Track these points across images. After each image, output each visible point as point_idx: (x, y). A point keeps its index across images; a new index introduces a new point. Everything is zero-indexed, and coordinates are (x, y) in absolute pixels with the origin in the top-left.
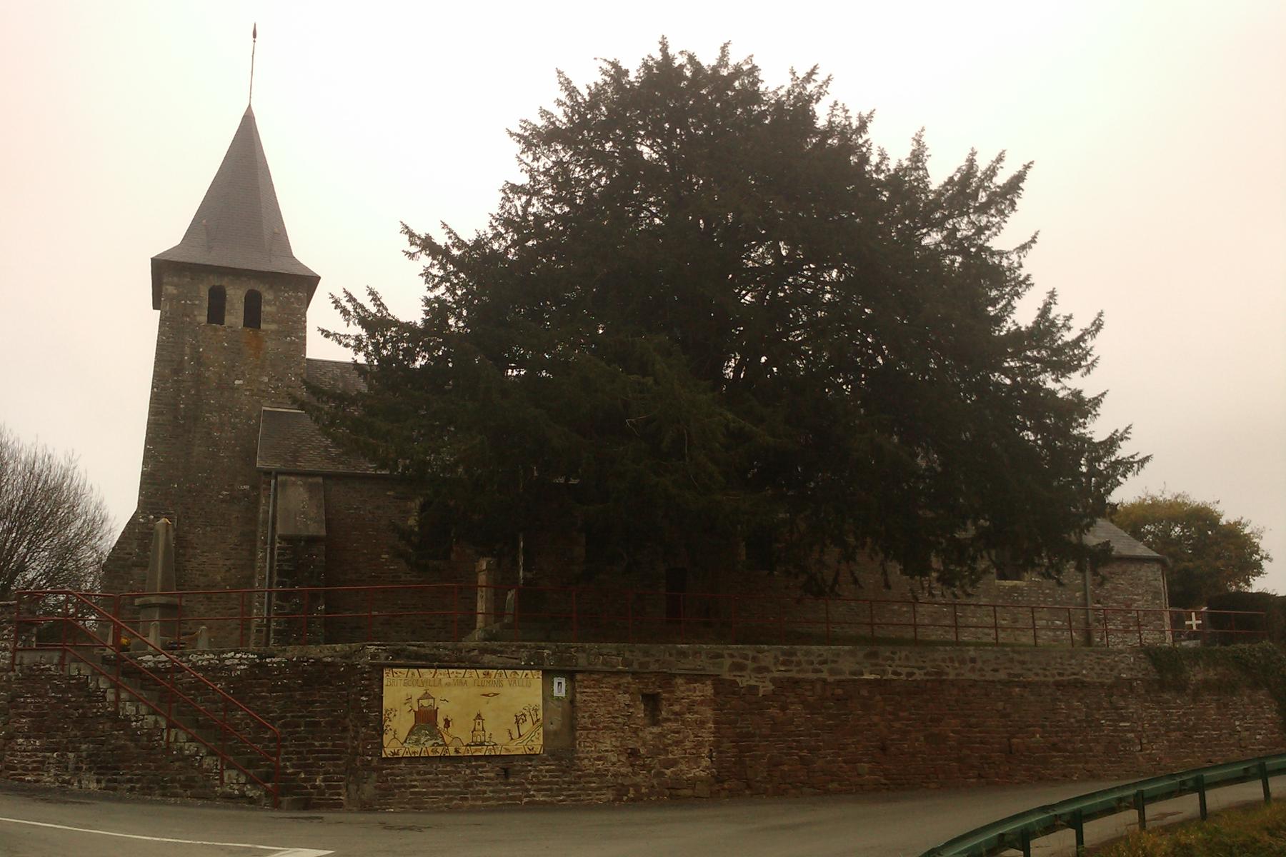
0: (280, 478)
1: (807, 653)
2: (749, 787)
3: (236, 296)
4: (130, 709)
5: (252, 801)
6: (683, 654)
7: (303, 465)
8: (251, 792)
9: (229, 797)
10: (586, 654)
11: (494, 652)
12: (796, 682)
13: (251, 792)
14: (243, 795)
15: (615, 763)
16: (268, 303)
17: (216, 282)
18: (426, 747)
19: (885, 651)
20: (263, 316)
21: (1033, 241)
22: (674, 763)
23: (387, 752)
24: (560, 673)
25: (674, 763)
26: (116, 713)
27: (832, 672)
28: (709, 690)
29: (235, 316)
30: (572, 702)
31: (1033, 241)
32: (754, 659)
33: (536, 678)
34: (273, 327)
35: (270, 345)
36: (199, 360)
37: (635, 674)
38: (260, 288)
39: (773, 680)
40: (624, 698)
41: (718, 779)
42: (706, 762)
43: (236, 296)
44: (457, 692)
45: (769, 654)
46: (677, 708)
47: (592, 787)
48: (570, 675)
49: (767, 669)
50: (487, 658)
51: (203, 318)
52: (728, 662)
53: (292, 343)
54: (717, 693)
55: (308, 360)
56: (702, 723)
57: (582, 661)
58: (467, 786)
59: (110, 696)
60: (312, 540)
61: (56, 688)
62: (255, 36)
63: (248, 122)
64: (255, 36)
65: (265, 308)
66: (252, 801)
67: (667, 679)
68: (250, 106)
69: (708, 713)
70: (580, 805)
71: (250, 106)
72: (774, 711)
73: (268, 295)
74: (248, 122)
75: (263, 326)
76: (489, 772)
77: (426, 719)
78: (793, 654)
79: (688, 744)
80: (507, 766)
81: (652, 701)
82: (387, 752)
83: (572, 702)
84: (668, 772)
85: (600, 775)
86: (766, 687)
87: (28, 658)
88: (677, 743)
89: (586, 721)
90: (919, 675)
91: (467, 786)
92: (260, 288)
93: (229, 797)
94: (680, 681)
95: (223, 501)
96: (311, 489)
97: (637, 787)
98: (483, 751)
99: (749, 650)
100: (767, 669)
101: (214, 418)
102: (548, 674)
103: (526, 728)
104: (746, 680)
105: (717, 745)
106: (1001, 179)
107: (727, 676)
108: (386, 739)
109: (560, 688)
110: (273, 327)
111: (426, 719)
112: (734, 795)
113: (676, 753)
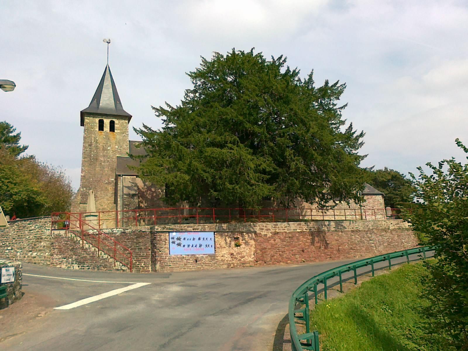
4: (87, 246)
15: (228, 258)
20: (115, 128)
22: (244, 257)
26: (83, 247)
29: (107, 128)
34: (119, 131)
42: (253, 256)
59: (81, 242)
61: (65, 241)
65: (116, 126)
73: (116, 121)
75: (116, 131)
86: (270, 235)
89: (219, 246)
101: (102, 159)
110: (119, 131)
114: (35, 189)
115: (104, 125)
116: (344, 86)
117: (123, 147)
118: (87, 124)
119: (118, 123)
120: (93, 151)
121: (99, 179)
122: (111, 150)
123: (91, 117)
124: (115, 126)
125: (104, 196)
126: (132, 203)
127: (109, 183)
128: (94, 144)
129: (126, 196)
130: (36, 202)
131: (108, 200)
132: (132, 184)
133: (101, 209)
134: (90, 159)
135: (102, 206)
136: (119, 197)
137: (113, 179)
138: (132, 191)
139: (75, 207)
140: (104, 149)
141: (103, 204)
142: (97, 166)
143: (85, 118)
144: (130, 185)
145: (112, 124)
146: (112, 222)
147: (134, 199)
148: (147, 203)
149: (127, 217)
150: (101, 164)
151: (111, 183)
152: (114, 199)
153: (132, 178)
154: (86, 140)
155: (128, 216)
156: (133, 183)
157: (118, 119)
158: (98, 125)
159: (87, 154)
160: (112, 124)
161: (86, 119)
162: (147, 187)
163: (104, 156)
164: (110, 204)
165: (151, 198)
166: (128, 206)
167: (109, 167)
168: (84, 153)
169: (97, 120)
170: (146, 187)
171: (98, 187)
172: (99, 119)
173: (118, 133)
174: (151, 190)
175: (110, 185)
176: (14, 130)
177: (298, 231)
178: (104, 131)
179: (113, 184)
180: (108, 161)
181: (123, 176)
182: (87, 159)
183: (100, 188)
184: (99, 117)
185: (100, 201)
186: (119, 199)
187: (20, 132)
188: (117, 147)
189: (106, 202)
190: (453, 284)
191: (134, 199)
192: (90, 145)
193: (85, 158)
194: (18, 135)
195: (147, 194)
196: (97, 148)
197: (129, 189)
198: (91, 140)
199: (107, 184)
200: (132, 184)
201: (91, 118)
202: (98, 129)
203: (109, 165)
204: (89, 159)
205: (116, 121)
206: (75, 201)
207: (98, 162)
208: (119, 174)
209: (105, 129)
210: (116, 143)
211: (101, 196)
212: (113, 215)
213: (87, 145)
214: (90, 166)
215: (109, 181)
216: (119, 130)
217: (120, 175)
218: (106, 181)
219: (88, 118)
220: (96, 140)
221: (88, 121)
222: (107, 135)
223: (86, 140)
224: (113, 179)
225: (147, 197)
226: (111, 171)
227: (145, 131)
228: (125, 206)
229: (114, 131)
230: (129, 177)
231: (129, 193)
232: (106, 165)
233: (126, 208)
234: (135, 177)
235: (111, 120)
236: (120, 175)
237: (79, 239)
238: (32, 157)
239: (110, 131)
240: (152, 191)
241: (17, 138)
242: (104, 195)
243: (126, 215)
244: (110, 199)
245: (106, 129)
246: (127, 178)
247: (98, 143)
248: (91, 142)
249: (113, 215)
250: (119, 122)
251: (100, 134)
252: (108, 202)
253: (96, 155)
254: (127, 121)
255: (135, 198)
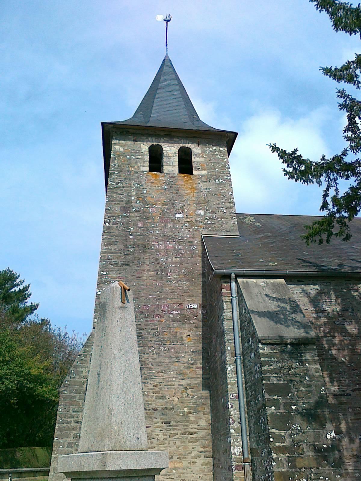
34: (204, 172)
73: (196, 149)
75: (195, 172)
101: (160, 246)
110: (204, 172)
114: (35, 372)
115: (165, 159)
117: (219, 213)
118: (119, 155)
119: (200, 152)
120: (135, 225)
121: (151, 307)
122: (184, 220)
123: (129, 140)
124: (193, 159)
125: (167, 361)
126: (298, 379)
127: (183, 319)
128: (136, 205)
129: (267, 350)
130: (38, 395)
131: (181, 375)
132: (282, 305)
133: (160, 408)
134: (126, 247)
135: (163, 397)
136: (229, 357)
137: (195, 306)
138: (288, 326)
139: (71, 404)
140: (165, 219)
141: (165, 391)
142: (146, 267)
143: (113, 142)
144: (273, 306)
146: (202, 460)
147: (302, 363)
148: (339, 382)
149: (285, 447)
150: (157, 259)
151: (189, 319)
152: (200, 372)
153: (273, 284)
154: (115, 195)
155: (288, 442)
156: (283, 300)
157: (199, 144)
158: (147, 158)
159: (117, 232)
161: (115, 144)
162: (328, 317)
163: (166, 238)
164: (189, 391)
165: (350, 361)
166: (285, 396)
167: (181, 269)
168: (107, 231)
169: (145, 147)
170: (323, 319)
171: (149, 334)
172: (150, 144)
173: (203, 176)
174: (344, 331)
175: (187, 326)
176: (22, 282)
178: (165, 171)
179: (197, 321)
180: (178, 253)
181: (239, 280)
182: (116, 247)
183: (154, 335)
184: (150, 139)
185: (158, 380)
186: (230, 368)
187: (29, 285)
188: (202, 213)
189: (176, 384)
191: (302, 363)
192: (126, 209)
194: (26, 288)
195: (334, 345)
196: (145, 216)
197: (276, 323)
198: (129, 195)
199: (178, 321)
200: (282, 305)
201: (130, 143)
202: (147, 169)
203: (181, 263)
204: (121, 246)
205: (196, 149)
206: (75, 384)
207: (147, 256)
208: (224, 271)
209: (166, 168)
210: (198, 203)
211: (159, 364)
212: (202, 433)
213: (117, 209)
214: (125, 267)
215: (185, 312)
216: (203, 169)
217: (227, 277)
218: (174, 312)
219: (122, 142)
220: (141, 196)
221: (121, 150)
222: (171, 182)
223: (115, 195)
224: (195, 306)
225: (334, 358)
226: (188, 280)
228: (270, 392)
229: (191, 173)
230: (260, 281)
231: (281, 337)
232: (173, 263)
233: (276, 404)
234: (283, 280)
235: (182, 145)
236: (227, 277)
238: (44, 322)
239: (180, 172)
240: (350, 335)
241: (23, 294)
242: (170, 358)
243: (281, 438)
244: (188, 371)
245: (170, 168)
246: (256, 285)
247: (146, 203)
248: (129, 201)
249: (202, 433)
250: (204, 152)
251: (153, 179)
252: (184, 382)
253: (142, 234)
254: (224, 149)
255: (308, 356)
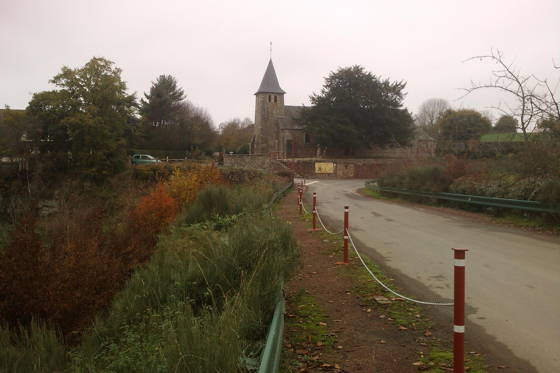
0: (285, 130)
1: (367, 160)
2: (358, 177)
3: (273, 97)
4: (285, 167)
5: (300, 178)
6: (350, 160)
7: (287, 128)
8: (300, 177)
9: (298, 177)
10: (338, 160)
11: (327, 160)
12: (365, 164)
13: (300, 177)
14: (299, 177)
15: (342, 174)
16: (278, 98)
17: (269, 94)
18: (320, 172)
19: (378, 159)
20: (277, 100)
21: (407, 93)
22: (349, 174)
23: (316, 173)
24: (335, 163)
25: (349, 174)
26: (283, 167)
27: (370, 163)
28: (353, 165)
29: (273, 101)
30: (336, 166)
31: (407, 93)
32: (360, 161)
33: (332, 164)
34: (279, 102)
35: (279, 105)
36: (268, 108)
37: (344, 163)
38: (276, 95)
39: (362, 164)
40: (343, 166)
41: (354, 177)
42: (353, 174)
43: (273, 97)
44: (323, 165)
45: (362, 160)
46: (349, 167)
47: (36, 367)
48: (336, 163)
49: (361, 162)
50: (326, 161)
51: (268, 101)
52: (356, 161)
53: (282, 105)
54: (354, 165)
55: (285, 106)
56: (352, 169)
57: (338, 162)
58: (324, 176)
59: (282, 165)
60: (291, 141)
61: (275, 165)
62: (271, 44)
63: (271, 63)
64: (271, 44)
65: (277, 99)
66: (300, 178)
67: (348, 164)
68: (271, 59)
69: (353, 168)
70: (337, 179)
71: (271, 59)
72: (362, 168)
73: (278, 96)
74: (271, 63)
75: (277, 102)
76: (327, 175)
77: (320, 169)
78: (365, 160)
79: (350, 172)
80: (329, 174)
81: (346, 167)
82: (316, 173)
83: (336, 166)
84: (348, 175)
85: (340, 176)
86: (361, 165)
87: (272, 161)
88: (349, 172)
89: (338, 169)
90: (383, 163)
91: (324, 176)
92: (276, 95)
93: (298, 177)
94: (350, 164)
95: (273, 132)
96: (289, 132)
97: (344, 177)
98: (326, 173)
99: (359, 160)
100: (361, 162)
101: (271, 118)
102: (334, 163)
103: (331, 169)
104: (358, 164)
105: (354, 172)
106: (402, 84)
107: (356, 163)
108: (316, 171)
109: (335, 165)
110: (279, 102)
111: (320, 169)
112: (356, 178)
113: (349, 173)
116: (65, 68)
140: (272, 113)
145: (276, 97)
160: (276, 97)
177: (375, 163)
190: (26, 159)
193: (262, 118)
227: (54, 92)
237: (281, 164)
